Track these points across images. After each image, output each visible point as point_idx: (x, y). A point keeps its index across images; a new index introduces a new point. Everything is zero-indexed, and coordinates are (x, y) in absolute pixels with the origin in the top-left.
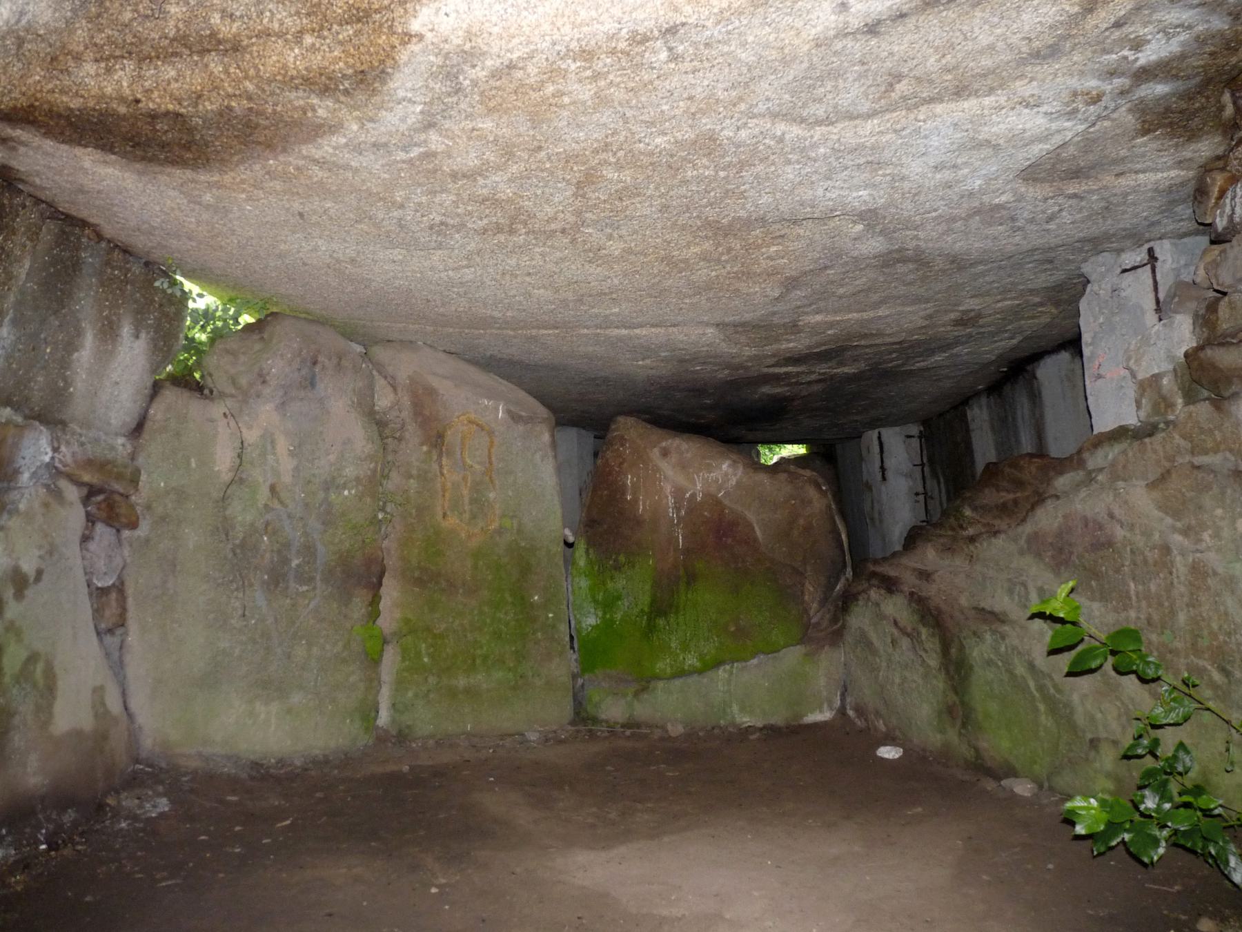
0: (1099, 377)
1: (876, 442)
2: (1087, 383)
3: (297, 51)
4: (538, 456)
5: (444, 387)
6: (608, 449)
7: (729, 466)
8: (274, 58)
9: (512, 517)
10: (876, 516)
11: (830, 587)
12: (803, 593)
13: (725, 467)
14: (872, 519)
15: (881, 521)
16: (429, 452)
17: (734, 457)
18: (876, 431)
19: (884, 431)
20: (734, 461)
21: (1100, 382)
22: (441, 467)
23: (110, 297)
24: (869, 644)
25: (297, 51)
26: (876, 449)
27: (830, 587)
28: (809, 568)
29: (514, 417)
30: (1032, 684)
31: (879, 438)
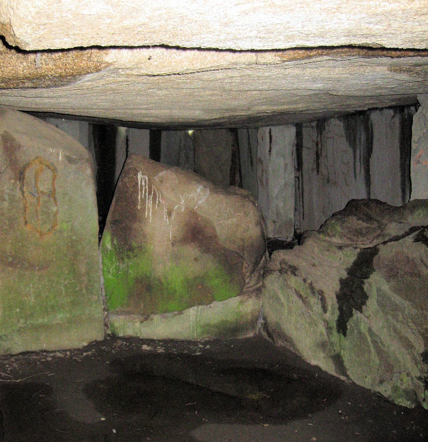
0: (418, 162)
1: (268, 135)
2: (412, 163)
3: (25, 64)
4: (83, 184)
5: (23, 140)
6: (125, 176)
7: (201, 190)
8: (10, 68)
9: (67, 222)
10: (264, 179)
11: (256, 263)
12: (242, 268)
13: (198, 190)
14: (261, 181)
15: (267, 183)
16: (15, 182)
17: (205, 183)
18: (269, 128)
19: (273, 128)
20: (205, 187)
21: (418, 165)
22: (23, 193)
23: (108, 436)
24: (278, 299)
25: (25, 64)
26: (268, 140)
27: (256, 263)
28: (246, 253)
29: (70, 160)
30: (369, 339)
31: (270, 132)
